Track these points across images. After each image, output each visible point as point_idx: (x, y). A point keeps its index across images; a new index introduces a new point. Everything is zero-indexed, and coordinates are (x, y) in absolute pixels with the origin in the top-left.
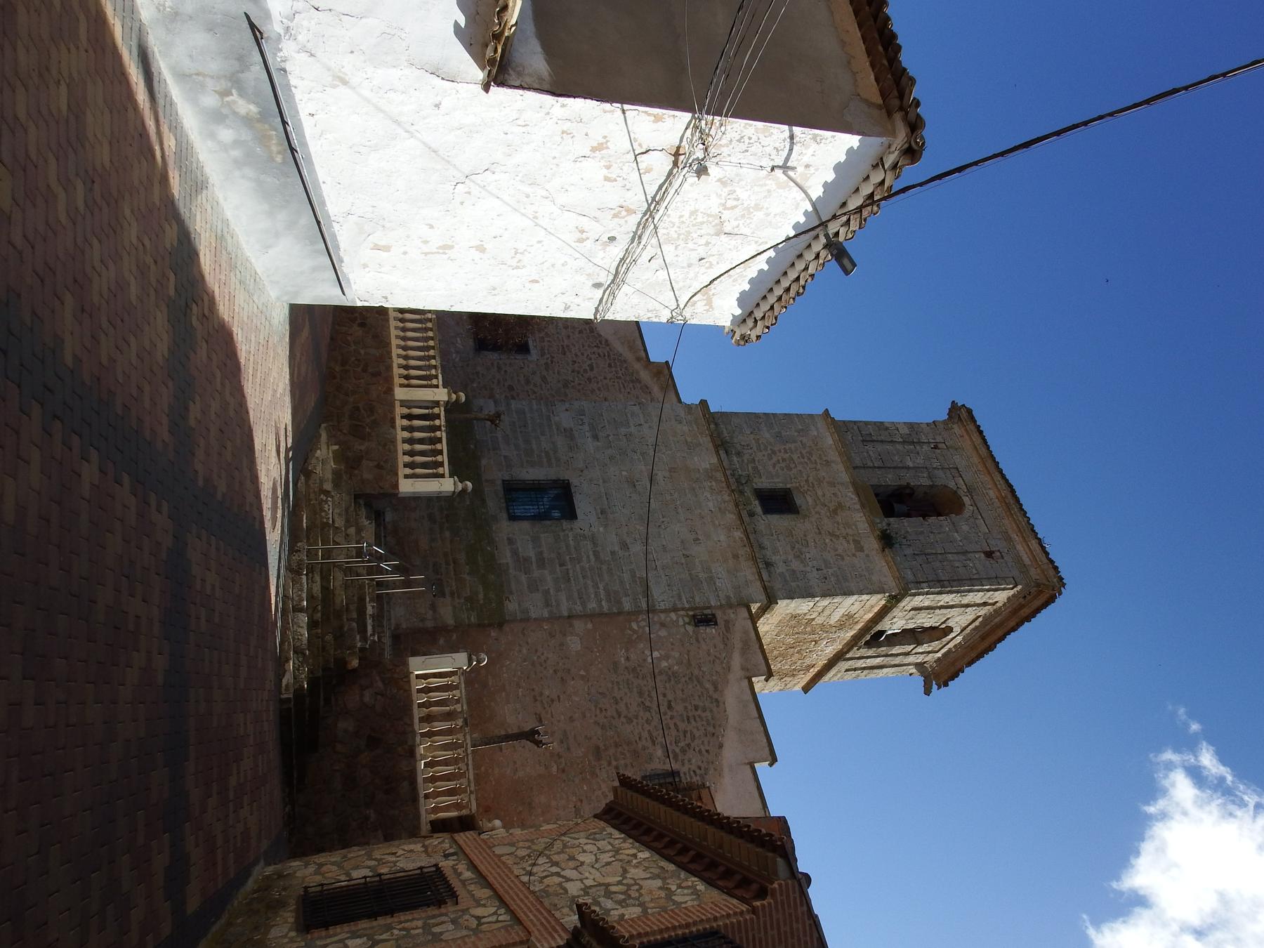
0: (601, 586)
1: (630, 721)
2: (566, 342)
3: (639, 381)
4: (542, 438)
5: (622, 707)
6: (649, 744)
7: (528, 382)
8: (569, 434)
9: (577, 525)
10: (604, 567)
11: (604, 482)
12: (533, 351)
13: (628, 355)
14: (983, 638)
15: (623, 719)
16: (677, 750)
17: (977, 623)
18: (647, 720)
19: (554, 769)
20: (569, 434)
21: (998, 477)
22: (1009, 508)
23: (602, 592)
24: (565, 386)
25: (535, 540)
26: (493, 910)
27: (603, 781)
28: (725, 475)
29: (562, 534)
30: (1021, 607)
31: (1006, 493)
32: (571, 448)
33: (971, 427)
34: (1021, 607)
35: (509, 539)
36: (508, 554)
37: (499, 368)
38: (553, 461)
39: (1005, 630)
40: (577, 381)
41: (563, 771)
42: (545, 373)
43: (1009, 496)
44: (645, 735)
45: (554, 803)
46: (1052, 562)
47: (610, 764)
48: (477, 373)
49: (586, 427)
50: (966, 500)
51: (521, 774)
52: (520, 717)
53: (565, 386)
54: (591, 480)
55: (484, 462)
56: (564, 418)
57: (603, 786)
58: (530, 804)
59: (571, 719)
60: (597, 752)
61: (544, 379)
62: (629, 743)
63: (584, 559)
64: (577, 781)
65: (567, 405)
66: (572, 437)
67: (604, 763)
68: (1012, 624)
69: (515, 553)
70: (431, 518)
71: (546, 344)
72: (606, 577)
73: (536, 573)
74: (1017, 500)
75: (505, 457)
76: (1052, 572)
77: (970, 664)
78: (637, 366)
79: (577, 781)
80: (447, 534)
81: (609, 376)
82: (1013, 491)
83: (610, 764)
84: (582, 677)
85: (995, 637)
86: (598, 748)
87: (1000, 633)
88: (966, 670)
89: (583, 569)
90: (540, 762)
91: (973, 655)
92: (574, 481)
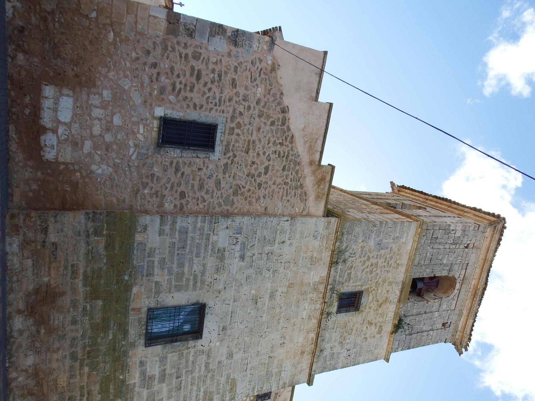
0: (202, 390)
2: (254, 137)
3: (302, 186)
4: (196, 260)
7: (201, 187)
8: (221, 254)
9: (199, 342)
10: (210, 375)
11: (235, 301)
12: (219, 148)
13: (305, 158)
20: (221, 254)
21: (484, 276)
23: (202, 394)
24: (235, 193)
25: (163, 360)
27: (181, 83)
28: (326, 288)
29: (185, 352)
31: (481, 287)
32: (217, 270)
35: (141, 362)
36: (137, 375)
37: (177, 170)
38: (199, 284)
40: (247, 187)
42: (221, 176)
43: (481, 290)
46: (471, 335)
48: (153, 175)
49: (238, 247)
50: (458, 286)
53: (235, 193)
54: (224, 300)
55: (135, 290)
56: (222, 237)
61: (218, 183)
63: (197, 370)
65: (229, 222)
66: (222, 258)
69: (143, 374)
70: (73, 357)
71: (234, 137)
72: (208, 382)
73: (156, 387)
74: (483, 294)
75: (156, 283)
76: (466, 340)
78: (307, 171)
80: (86, 369)
81: (279, 180)
82: (485, 289)
89: (193, 378)
92: (210, 303)
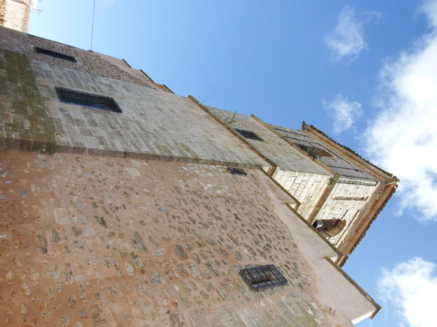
1: (206, 226)
5: (193, 216)
6: (232, 244)
14: (357, 232)
15: (197, 224)
16: (261, 249)
17: (358, 214)
18: (222, 227)
19: (130, 269)
22: (350, 156)
26: (34, 61)
30: (377, 202)
33: (315, 131)
34: (377, 202)
39: (370, 220)
41: (143, 272)
44: (225, 237)
45: (135, 311)
47: (199, 262)
51: (78, 278)
52: (75, 219)
57: (199, 285)
58: (96, 316)
59: (142, 223)
60: (181, 252)
62: (213, 243)
64: (164, 281)
67: (193, 262)
68: (373, 215)
77: (351, 252)
79: (164, 281)
83: (199, 262)
84: (147, 194)
85: (363, 228)
86: (180, 248)
87: (366, 224)
88: (350, 256)
90: (108, 263)
91: (353, 244)
